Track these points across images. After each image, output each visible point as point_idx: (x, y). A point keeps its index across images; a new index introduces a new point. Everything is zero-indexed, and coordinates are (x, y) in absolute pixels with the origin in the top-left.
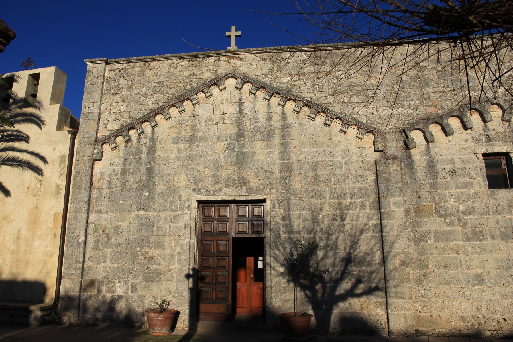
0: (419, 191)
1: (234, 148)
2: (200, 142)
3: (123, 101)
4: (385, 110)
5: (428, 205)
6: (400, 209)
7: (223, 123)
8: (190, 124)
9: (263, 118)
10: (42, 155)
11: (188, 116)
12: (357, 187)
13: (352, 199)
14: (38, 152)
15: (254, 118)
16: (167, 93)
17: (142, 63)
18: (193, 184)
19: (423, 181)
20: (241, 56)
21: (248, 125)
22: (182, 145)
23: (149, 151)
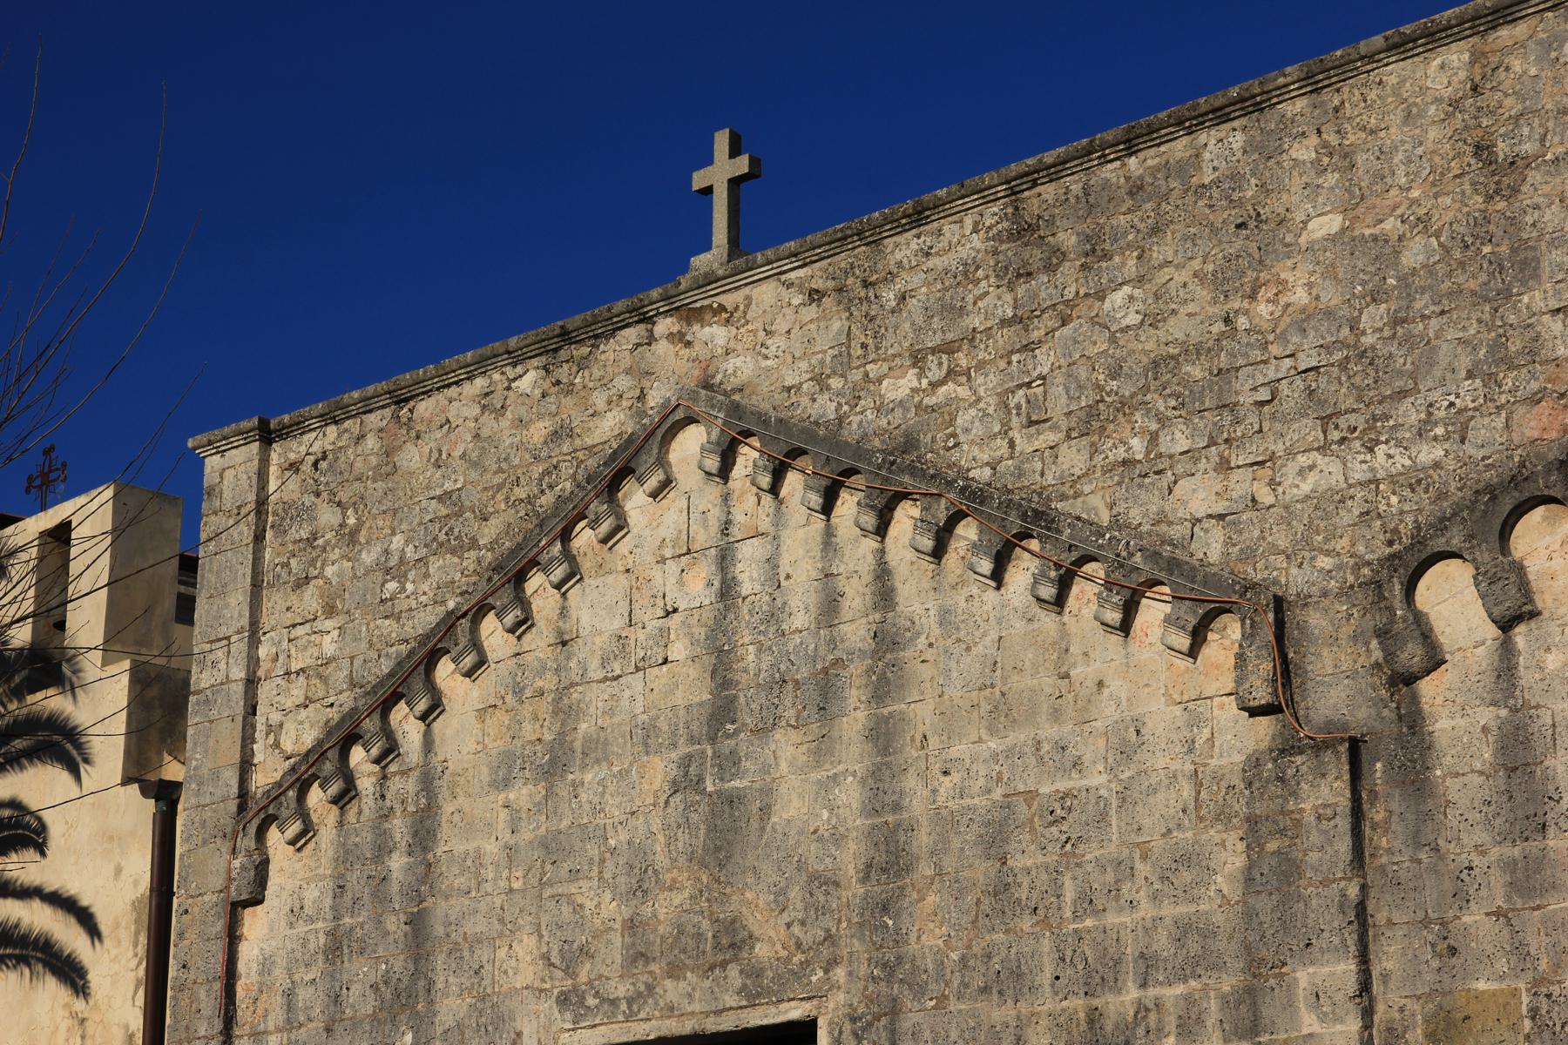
0: (1451, 913)
1: (701, 780)
2: (584, 767)
3: (330, 611)
4: (1311, 468)
5: (1494, 994)
6: (1339, 1027)
7: (666, 661)
8: (548, 682)
9: (807, 610)
10: (84, 902)
11: (543, 644)
12: (1168, 921)
13: (1144, 985)
14: (72, 892)
15: (774, 616)
16: (474, 544)
17: (387, 412)
18: (560, 974)
19: (1474, 856)
20: (728, 300)
21: (751, 657)
22: (523, 794)
23: (416, 834)
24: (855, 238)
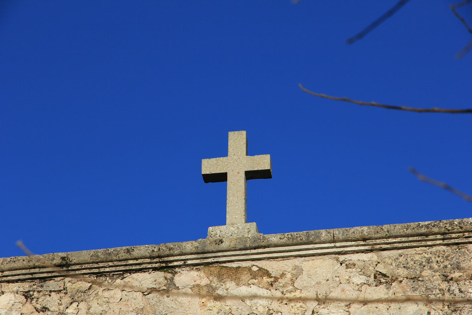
24: (439, 237)
